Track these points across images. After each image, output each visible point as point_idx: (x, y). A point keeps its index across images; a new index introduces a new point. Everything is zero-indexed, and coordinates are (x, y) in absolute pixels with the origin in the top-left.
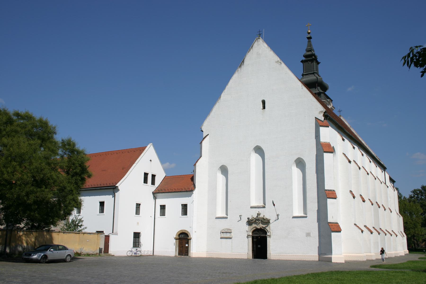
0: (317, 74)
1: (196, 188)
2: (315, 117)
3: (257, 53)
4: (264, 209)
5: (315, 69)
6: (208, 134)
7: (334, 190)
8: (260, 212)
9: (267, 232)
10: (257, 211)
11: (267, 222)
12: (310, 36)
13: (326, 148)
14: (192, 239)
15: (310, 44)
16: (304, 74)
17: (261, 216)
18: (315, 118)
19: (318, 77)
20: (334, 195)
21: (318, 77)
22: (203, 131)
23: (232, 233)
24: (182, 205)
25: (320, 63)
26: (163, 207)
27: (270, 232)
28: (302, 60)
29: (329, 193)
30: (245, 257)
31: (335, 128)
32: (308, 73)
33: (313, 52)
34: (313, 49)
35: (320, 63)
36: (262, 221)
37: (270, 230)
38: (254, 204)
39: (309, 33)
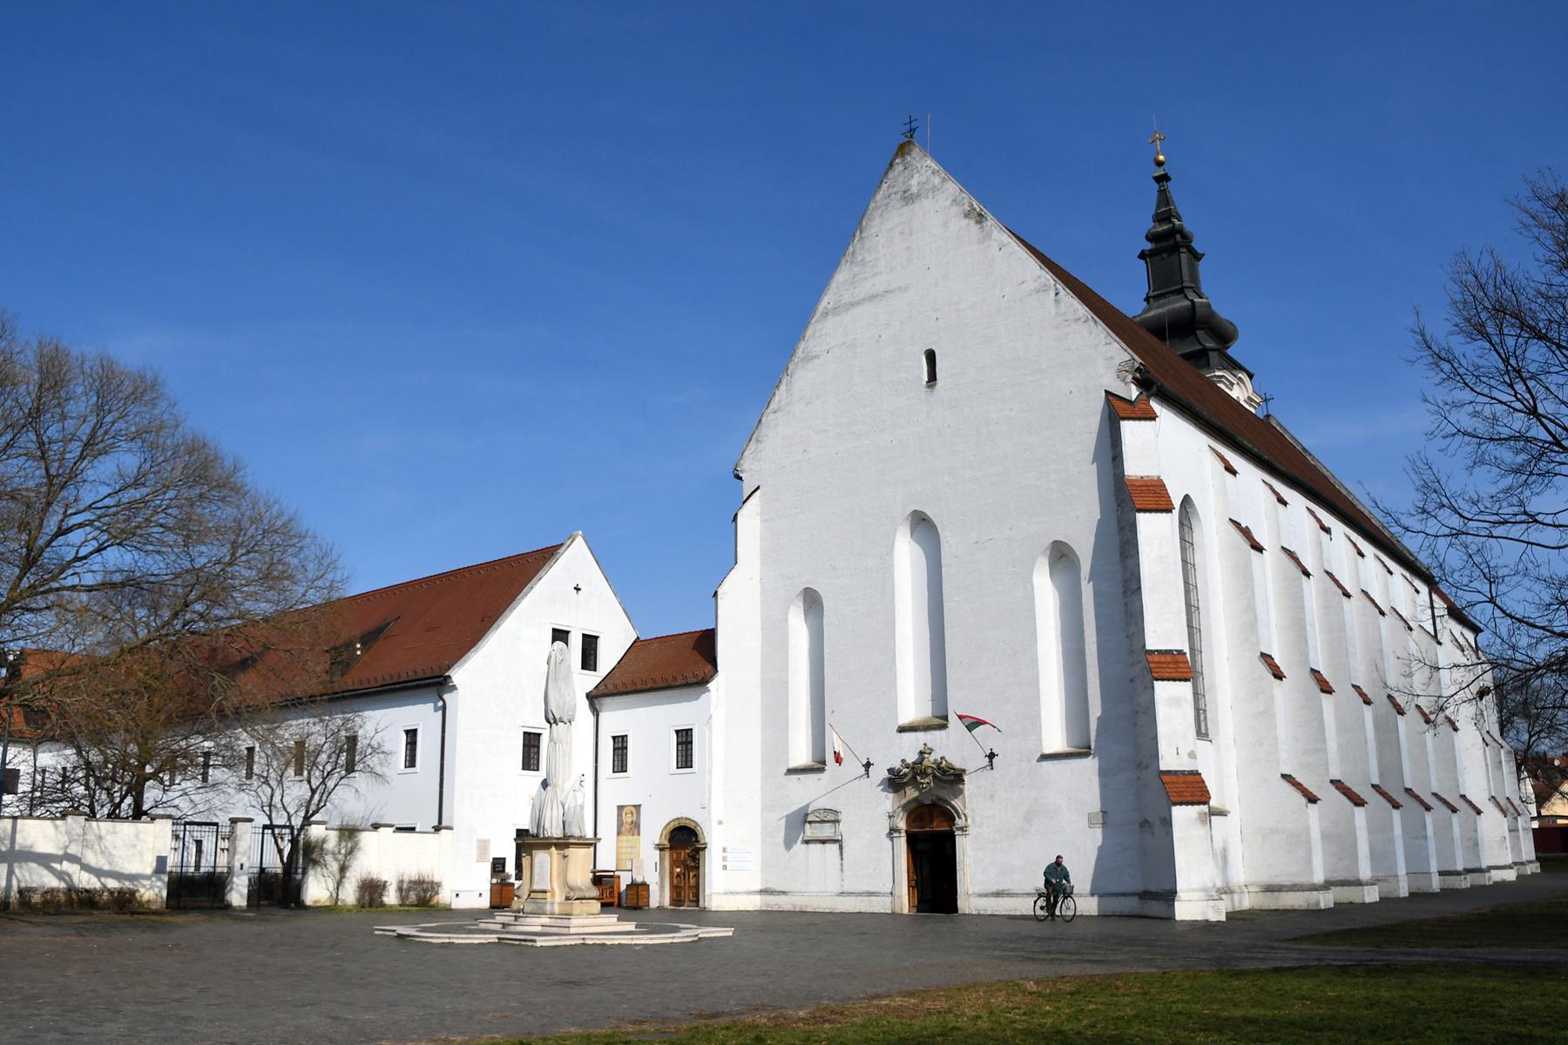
0: (1194, 292)
2: (1106, 391)
3: (905, 192)
4: (943, 732)
5: (1186, 277)
6: (758, 488)
7: (1181, 651)
8: (929, 746)
9: (953, 811)
10: (921, 738)
11: (952, 778)
12: (1163, 172)
13: (1146, 499)
14: (708, 846)
15: (1164, 198)
16: (1151, 294)
17: (930, 759)
18: (1104, 394)
19: (1197, 300)
20: (1179, 670)
21: (1197, 300)
22: (740, 478)
23: (841, 824)
24: (677, 732)
25: (1203, 255)
26: (620, 744)
27: (964, 814)
28: (1143, 251)
29: (1163, 663)
30: (881, 905)
31: (1193, 422)
33: (1177, 222)
34: (1177, 212)
35: (1203, 255)
36: (935, 777)
37: (965, 807)
38: (906, 718)
39: (1160, 164)
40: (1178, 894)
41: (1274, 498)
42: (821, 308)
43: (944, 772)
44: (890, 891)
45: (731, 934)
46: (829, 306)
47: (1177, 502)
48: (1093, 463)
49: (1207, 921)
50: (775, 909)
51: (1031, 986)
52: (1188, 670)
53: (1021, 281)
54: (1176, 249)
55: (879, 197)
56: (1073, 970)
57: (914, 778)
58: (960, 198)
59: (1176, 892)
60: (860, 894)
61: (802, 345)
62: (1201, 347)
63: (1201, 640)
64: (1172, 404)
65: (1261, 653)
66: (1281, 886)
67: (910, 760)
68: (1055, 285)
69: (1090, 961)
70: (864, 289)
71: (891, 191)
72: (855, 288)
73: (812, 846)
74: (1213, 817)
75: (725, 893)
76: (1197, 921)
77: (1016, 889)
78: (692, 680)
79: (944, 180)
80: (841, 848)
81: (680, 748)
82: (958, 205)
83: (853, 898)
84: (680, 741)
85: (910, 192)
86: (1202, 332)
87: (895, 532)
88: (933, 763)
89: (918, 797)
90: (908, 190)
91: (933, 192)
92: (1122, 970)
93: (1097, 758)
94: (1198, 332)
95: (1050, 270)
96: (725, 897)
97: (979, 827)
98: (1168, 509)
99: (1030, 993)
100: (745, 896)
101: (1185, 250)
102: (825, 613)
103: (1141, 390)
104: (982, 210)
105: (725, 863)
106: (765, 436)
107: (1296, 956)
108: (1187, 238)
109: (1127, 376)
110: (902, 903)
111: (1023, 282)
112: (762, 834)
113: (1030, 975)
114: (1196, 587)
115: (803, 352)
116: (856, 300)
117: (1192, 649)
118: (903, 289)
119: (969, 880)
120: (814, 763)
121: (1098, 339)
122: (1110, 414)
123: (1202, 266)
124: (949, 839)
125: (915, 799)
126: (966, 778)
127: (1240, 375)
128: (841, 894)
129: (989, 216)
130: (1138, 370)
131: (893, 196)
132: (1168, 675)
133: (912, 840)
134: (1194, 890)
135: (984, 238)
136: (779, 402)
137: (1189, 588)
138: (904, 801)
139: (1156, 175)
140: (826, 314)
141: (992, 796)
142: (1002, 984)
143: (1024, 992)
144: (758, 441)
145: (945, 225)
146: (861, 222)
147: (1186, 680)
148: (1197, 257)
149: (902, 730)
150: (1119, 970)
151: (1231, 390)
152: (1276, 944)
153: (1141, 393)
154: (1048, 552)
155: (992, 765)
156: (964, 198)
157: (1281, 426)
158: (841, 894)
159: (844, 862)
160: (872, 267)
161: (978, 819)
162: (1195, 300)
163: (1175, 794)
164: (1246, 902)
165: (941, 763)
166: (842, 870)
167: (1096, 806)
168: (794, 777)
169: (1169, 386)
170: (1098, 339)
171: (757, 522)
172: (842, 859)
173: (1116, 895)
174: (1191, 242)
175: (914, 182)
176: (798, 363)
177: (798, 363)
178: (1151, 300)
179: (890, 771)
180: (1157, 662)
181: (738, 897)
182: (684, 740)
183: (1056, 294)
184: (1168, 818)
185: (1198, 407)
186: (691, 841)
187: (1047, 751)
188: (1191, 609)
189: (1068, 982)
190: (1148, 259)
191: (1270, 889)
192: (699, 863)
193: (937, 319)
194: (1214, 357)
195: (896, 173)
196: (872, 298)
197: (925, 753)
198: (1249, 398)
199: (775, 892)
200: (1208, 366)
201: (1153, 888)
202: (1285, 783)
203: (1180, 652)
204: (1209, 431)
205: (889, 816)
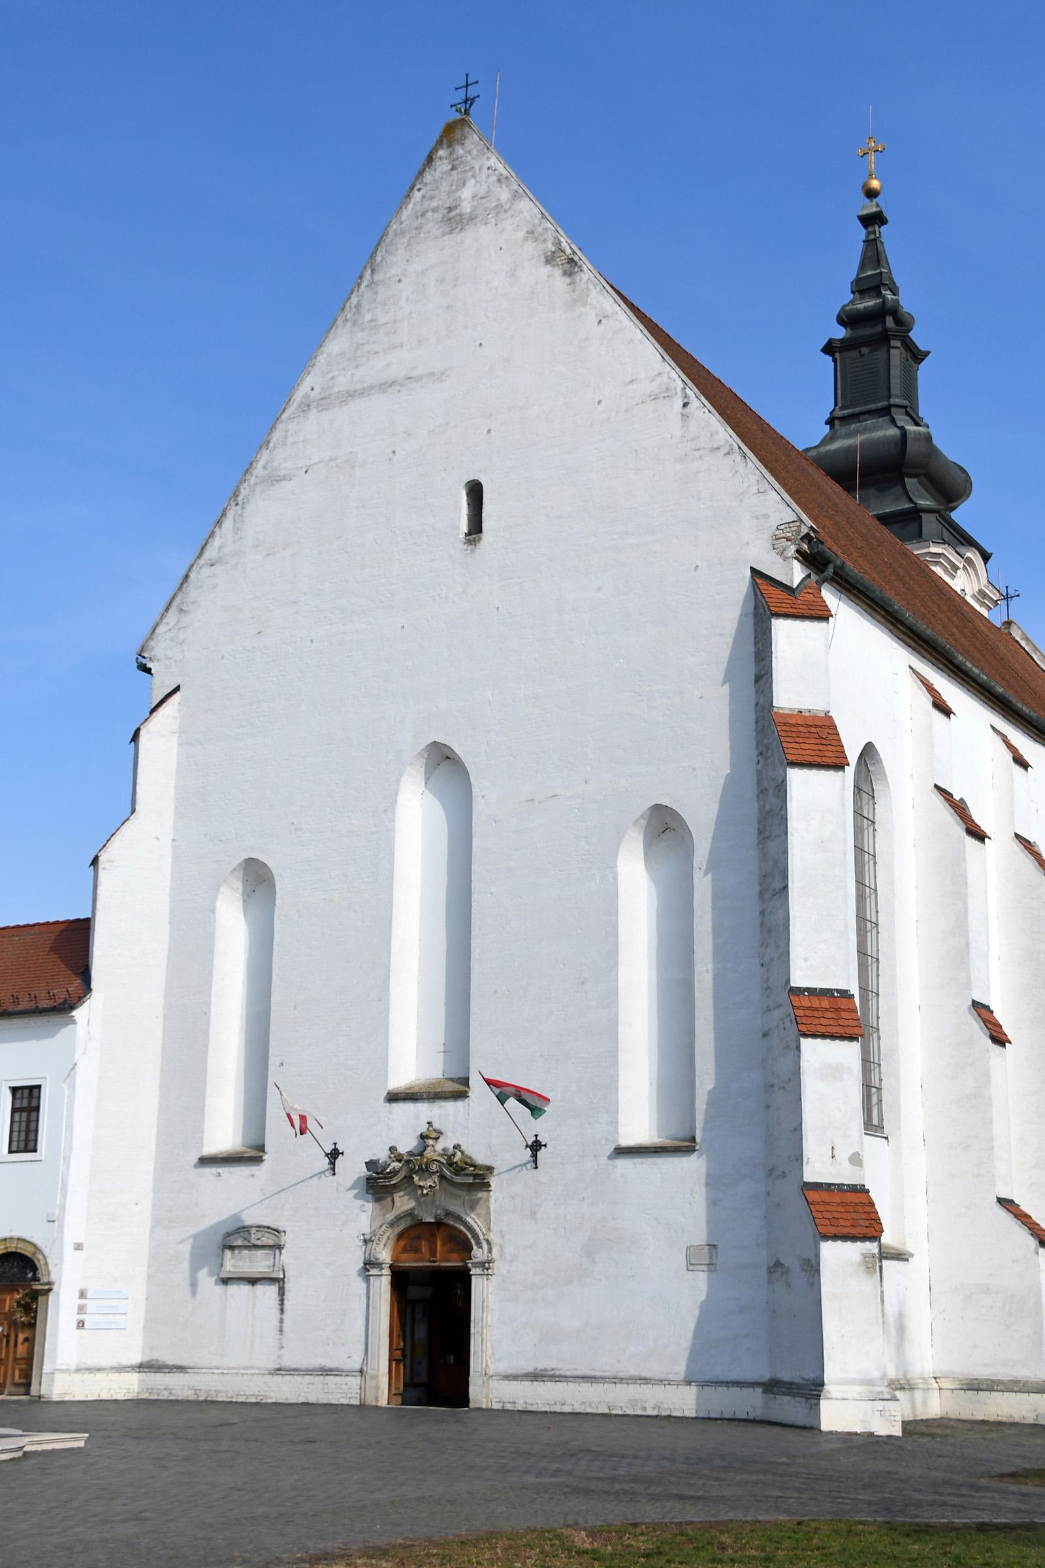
0: (908, 414)
1: (94, 993)
2: (752, 568)
3: (450, 209)
4: (460, 1105)
5: (896, 389)
6: (177, 689)
7: (846, 991)
8: (436, 1125)
9: (473, 1241)
12: (875, 209)
13: (803, 746)
14: (55, 1288)
15: (873, 253)
16: (839, 413)
18: (748, 574)
19: (911, 428)
20: (841, 1022)
21: (911, 428)
22: (148, 671)
24: (14, 1090)
27: (488, 1241)
28: (830, 341)
29: (817, 1009)
30: (343, 1391)
32: (857, 410)
36: (442, 1177)
38: (403, 1076)
39: (871, 194)
40: (827, 1387)
41: (1008, 756)
42: (298, 396)
43: (458, 1170)
44: (358, 1367)
45: (81, 1444)
46: (313, 394)
47: (853, 755)
48: (723, 684)
49: (871, 1434)
50: (164, 1396)
51: (582, 1540)
52: (855, 1023)
53: (629, 378)
54: (884, 339)
55: (406, 214)
56: (651, 1512)
57: (409, 1178)
58: (540, 229)
59: (822, 1384)
60: (308, 1372)
61: (265, 456)
62: (907, 505)
63: (878, 975)
64: (857, 597)
65: (974, 1002)
66: (993, 1381)
67: (403, 1149)
68: (684, 389)
69: (680, 1498)
70: (372, 371)
71: (426, 204)
72: (357, 367)
73: (233, 1289)
74: (885, 1262)
75: (78, 1370)
76: (856, 1434)
77: (565, 1368)
78: (44, 1004)
79: (515, 196)
80: (282, 1292)
81: (17, 1118)
82: (536, 240)
83: (298, 1379)
84: (18, 1105)
85: (458, 211)
86: (914, 481)
87: (401, 775)
88: (442, 1155)
89: (413, 1209)
90: (456, 207)
91: (497, 214)
92: (731, 1515)
93: (704, 1157)
94: (906, 479)
95: (678, 364)
96: (78, 1376)
97: (511, 1261)
98: (839, 765)
99: (581, 1553)
100: (113, 1376)
101: (898, 344)
102: (277, 902)
103: (808, 572)
104: (574, 252)
105: (82, 1317)
106: (194, 602)
107: (1014, 1505)
108: (904, 324)
109: (789, 546)
110: (377, 1388)
111: (632, 381)
112: (149, 1266)
113: (581, 1521)
114: (876, 890)
115: (265, 468)
116: (358, 387)
117: (864, 989)
118: (438, 376)
119: (489, 1352)
120: (244, 1149)
121: (746, 484)
122: (756, 607)
123: (924, 371)
124: (462, 1279)
125: (410, 1214)
126: (494, 1181)
127: (969, 554)
128: (278, 1371)
129: (586, 265)
130: (807, 538)
131: (430, 214)
132: (822, 1029)
133: (401, 1279)
134: (853, 1382)
135: (575, 301)
136: (220, 548)
137: (864, 891)
138: (390, 1216)
139: (865, 212)
140: (306, 407)
141: (533, 1213)
142: (535, 1535)
143: (570, 1550)
144: (181, 610)
145: (512, 274)
146: (373, 256)
147: (852, 1038)
148: (918, 356)
149: (394, 1098)
150: (725, 1515)
151: (953, 577)
152: (984, 1482)
153: (809, 576)
154: (644, 822)
155: (535, 1161)
156: (546, 229)
157: (1027, 639)
158: (278, 1371)
159: (285, 1316)
160: (387, 334)
161: (509, 1250)
162: (908, 427)
163: (827, 1222)
164: (934, 1406)
165: (454, 1155)
166: (281, 1331)
167: (700, 1237)
168: (210, 1171)
169: (854, 567)
170: (746, 484)
171: (173, 744)
172: (282, 1311)
173: (728, 1384)
174: (910, 331)
175: (466, 193)
176: (255, 484)
177: (255, 484)
178: (837, 422)
179: (371, 1165)
180: (808, 1008)
181: (100, 1376)
182: (25, 1104)
183: (685, 405)
184: (813, 1262)
185: (897, 605)
186: (24, 1279)
187: (625, 1142)
188: (865, 925)
189: (642, 1534)
190: (837, 356)
191: (974, 1386)
192: (35, 1317)
193: (489, 431)
194: (930, 523)
195: (437, 174)
196: (385, 386)
197: (428, 1137)
198: (981, 592)
199: (166, 1367)
200: (919, 536)
201: (786, 1377)
202: (1002, 1213)
203: (845, 994)
204: (913, 644)
205: (365, 1241)
